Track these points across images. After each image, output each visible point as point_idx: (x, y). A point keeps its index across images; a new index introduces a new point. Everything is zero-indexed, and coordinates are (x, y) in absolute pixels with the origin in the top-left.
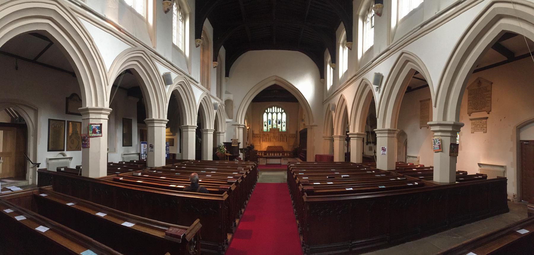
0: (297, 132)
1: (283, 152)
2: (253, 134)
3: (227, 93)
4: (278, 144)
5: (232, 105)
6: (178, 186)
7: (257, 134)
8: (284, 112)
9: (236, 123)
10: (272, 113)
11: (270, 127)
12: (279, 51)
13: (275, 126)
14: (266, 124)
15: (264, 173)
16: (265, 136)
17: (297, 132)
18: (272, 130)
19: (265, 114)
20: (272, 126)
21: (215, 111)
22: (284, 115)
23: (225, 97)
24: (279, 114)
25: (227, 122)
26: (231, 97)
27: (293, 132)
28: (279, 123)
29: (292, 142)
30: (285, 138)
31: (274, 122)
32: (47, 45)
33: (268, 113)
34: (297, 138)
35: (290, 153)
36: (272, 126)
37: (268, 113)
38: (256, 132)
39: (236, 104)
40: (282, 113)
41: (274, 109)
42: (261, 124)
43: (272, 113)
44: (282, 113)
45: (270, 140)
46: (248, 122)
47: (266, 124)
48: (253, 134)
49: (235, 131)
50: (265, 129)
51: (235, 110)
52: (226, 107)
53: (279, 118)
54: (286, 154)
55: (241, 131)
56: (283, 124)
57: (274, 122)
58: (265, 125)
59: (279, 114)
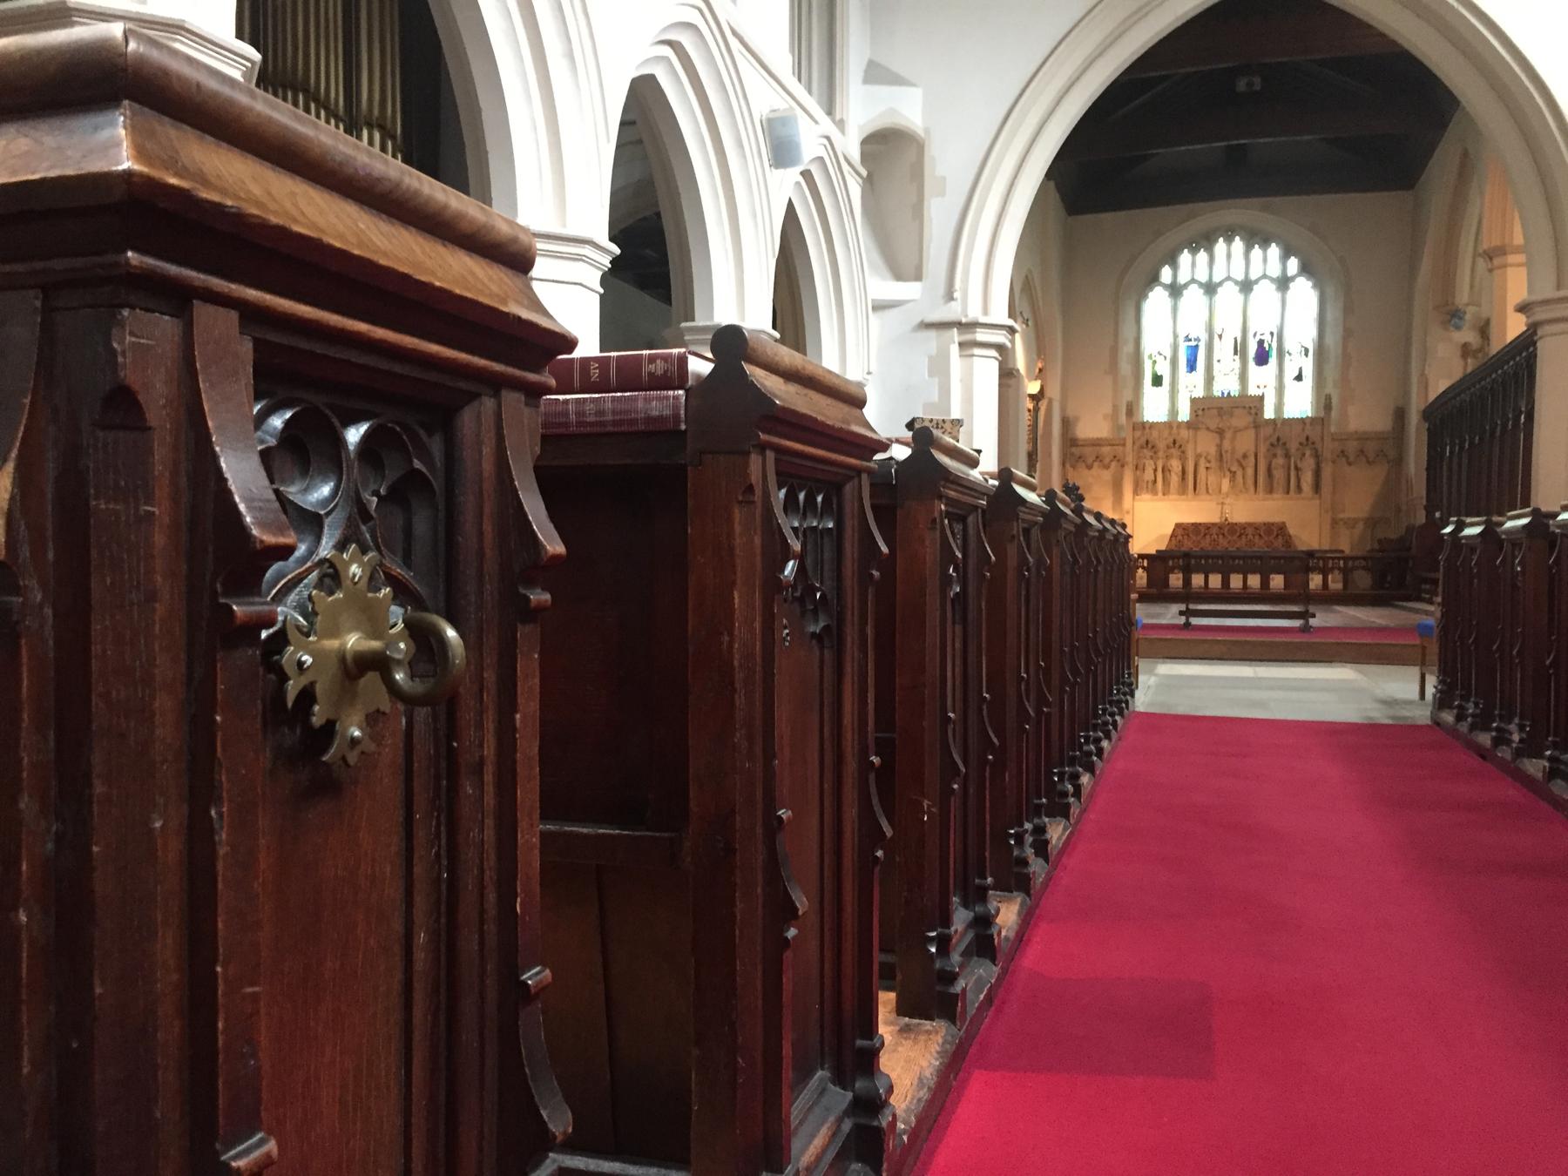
0: (1400, 415)
1: (1298, 563)
2: (1070, 441)
3: (876, 74)
4: (1246, 509)
5: (917, 173)
6: (51, 545)
7: (1097, 443)
8: (1305, 269)
9: (952, 312)
10: (1210, 289)
11: (1192, 386)
12: (1159, 209)
13: (1226, 384)
14: (1164, 369)
15: (1167, 669)
16: (1153, 453)
17: (1400, 415)
18: (1210, 410)
19: (1157, 299)
20: (1209, 379)
21: (784, 184)
22: (1304, 294)
23: (865, 107)
24: (1265, 293)
25: (879, 307)
26: (907, 108)
27: (1367, 417)
28: (1262, 358)
29: (1359, 494)
30: (1308, 464)
31: (1224, 350)
32: (211, 309)
33: (1175, 290)
34: (1399, 461)
35: (1347, 566)
36: (1209, 379)
37: (1175, 290)
38: (1093, 427)
39: (949, 162)
40: (1283, 283)
41: (1230, 257)
42: (1125, 368)
43: (1210, 289)
44: (1283, 283)
45: (1190, 484)
46: (1039, 347)
47: (1164, 369)
48: (1070, 441)
49: (939, 367)
50: (1154, 407)
51: (939, 214)
52: (869, 183)
53: (1263, 325)
54: (1315, 581)
55: (986, 370)
56: (1290, 372)
57: (1224, 350)
58: (1157, 381)
59: (1265, 293)
